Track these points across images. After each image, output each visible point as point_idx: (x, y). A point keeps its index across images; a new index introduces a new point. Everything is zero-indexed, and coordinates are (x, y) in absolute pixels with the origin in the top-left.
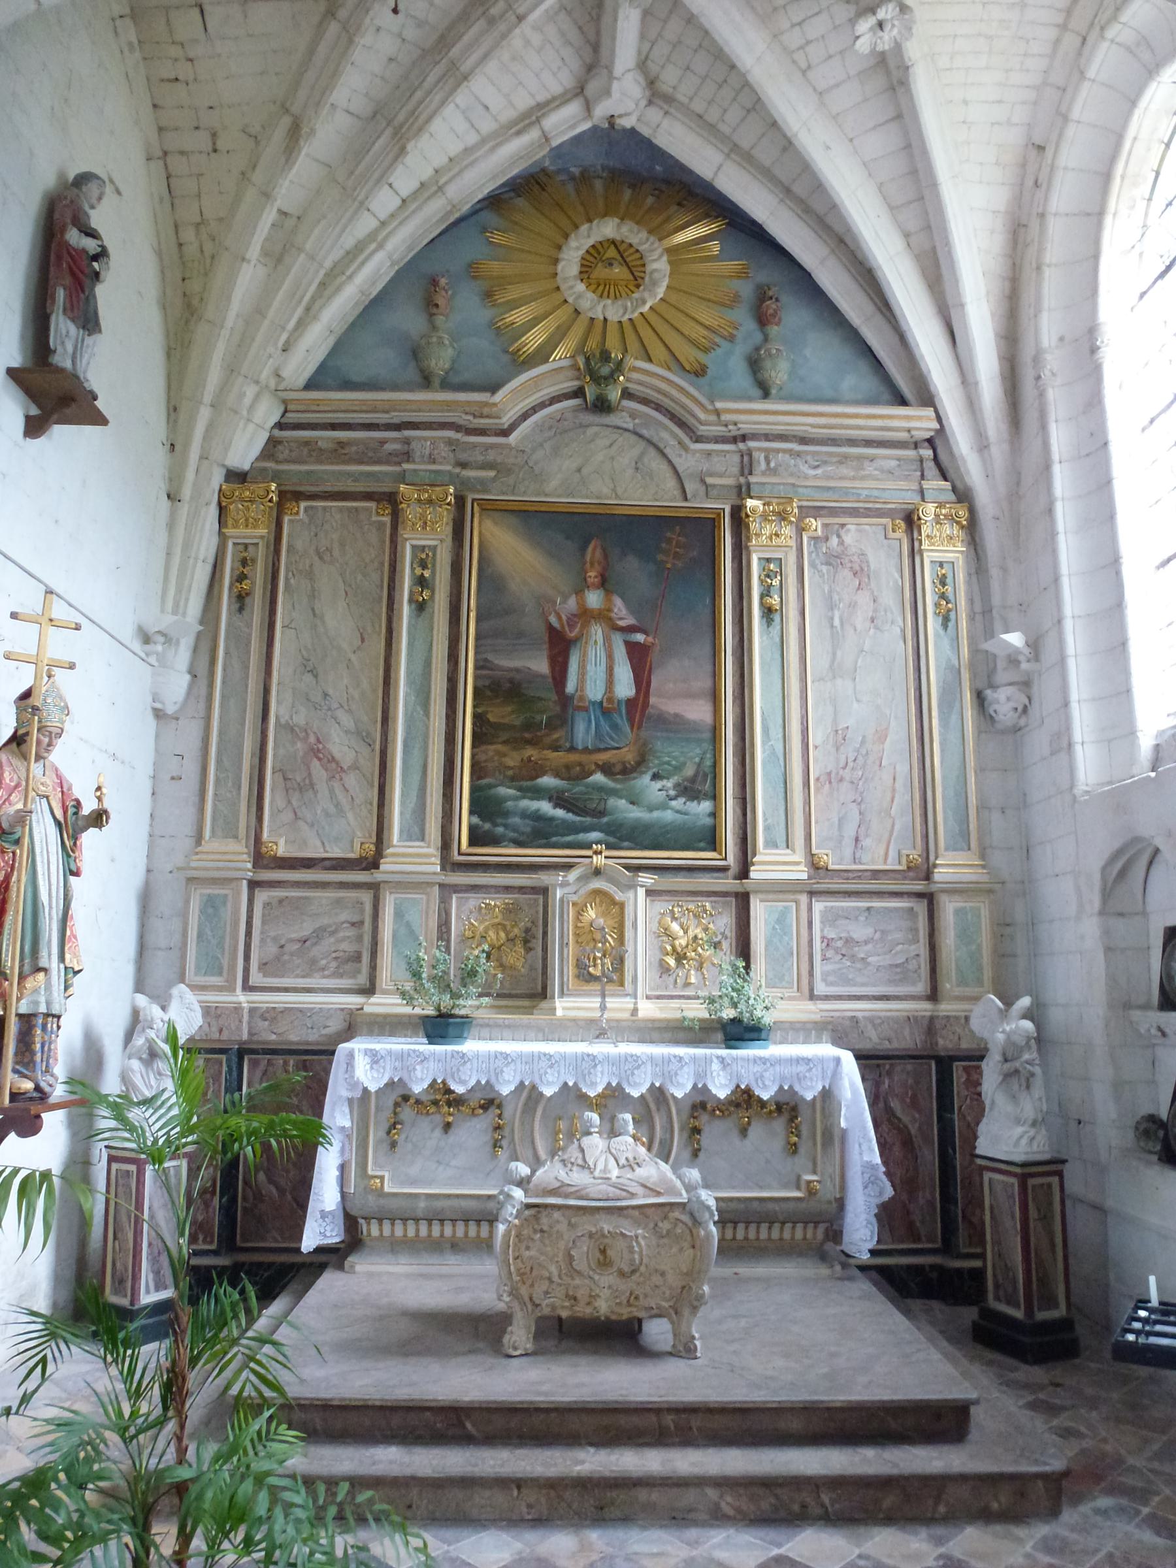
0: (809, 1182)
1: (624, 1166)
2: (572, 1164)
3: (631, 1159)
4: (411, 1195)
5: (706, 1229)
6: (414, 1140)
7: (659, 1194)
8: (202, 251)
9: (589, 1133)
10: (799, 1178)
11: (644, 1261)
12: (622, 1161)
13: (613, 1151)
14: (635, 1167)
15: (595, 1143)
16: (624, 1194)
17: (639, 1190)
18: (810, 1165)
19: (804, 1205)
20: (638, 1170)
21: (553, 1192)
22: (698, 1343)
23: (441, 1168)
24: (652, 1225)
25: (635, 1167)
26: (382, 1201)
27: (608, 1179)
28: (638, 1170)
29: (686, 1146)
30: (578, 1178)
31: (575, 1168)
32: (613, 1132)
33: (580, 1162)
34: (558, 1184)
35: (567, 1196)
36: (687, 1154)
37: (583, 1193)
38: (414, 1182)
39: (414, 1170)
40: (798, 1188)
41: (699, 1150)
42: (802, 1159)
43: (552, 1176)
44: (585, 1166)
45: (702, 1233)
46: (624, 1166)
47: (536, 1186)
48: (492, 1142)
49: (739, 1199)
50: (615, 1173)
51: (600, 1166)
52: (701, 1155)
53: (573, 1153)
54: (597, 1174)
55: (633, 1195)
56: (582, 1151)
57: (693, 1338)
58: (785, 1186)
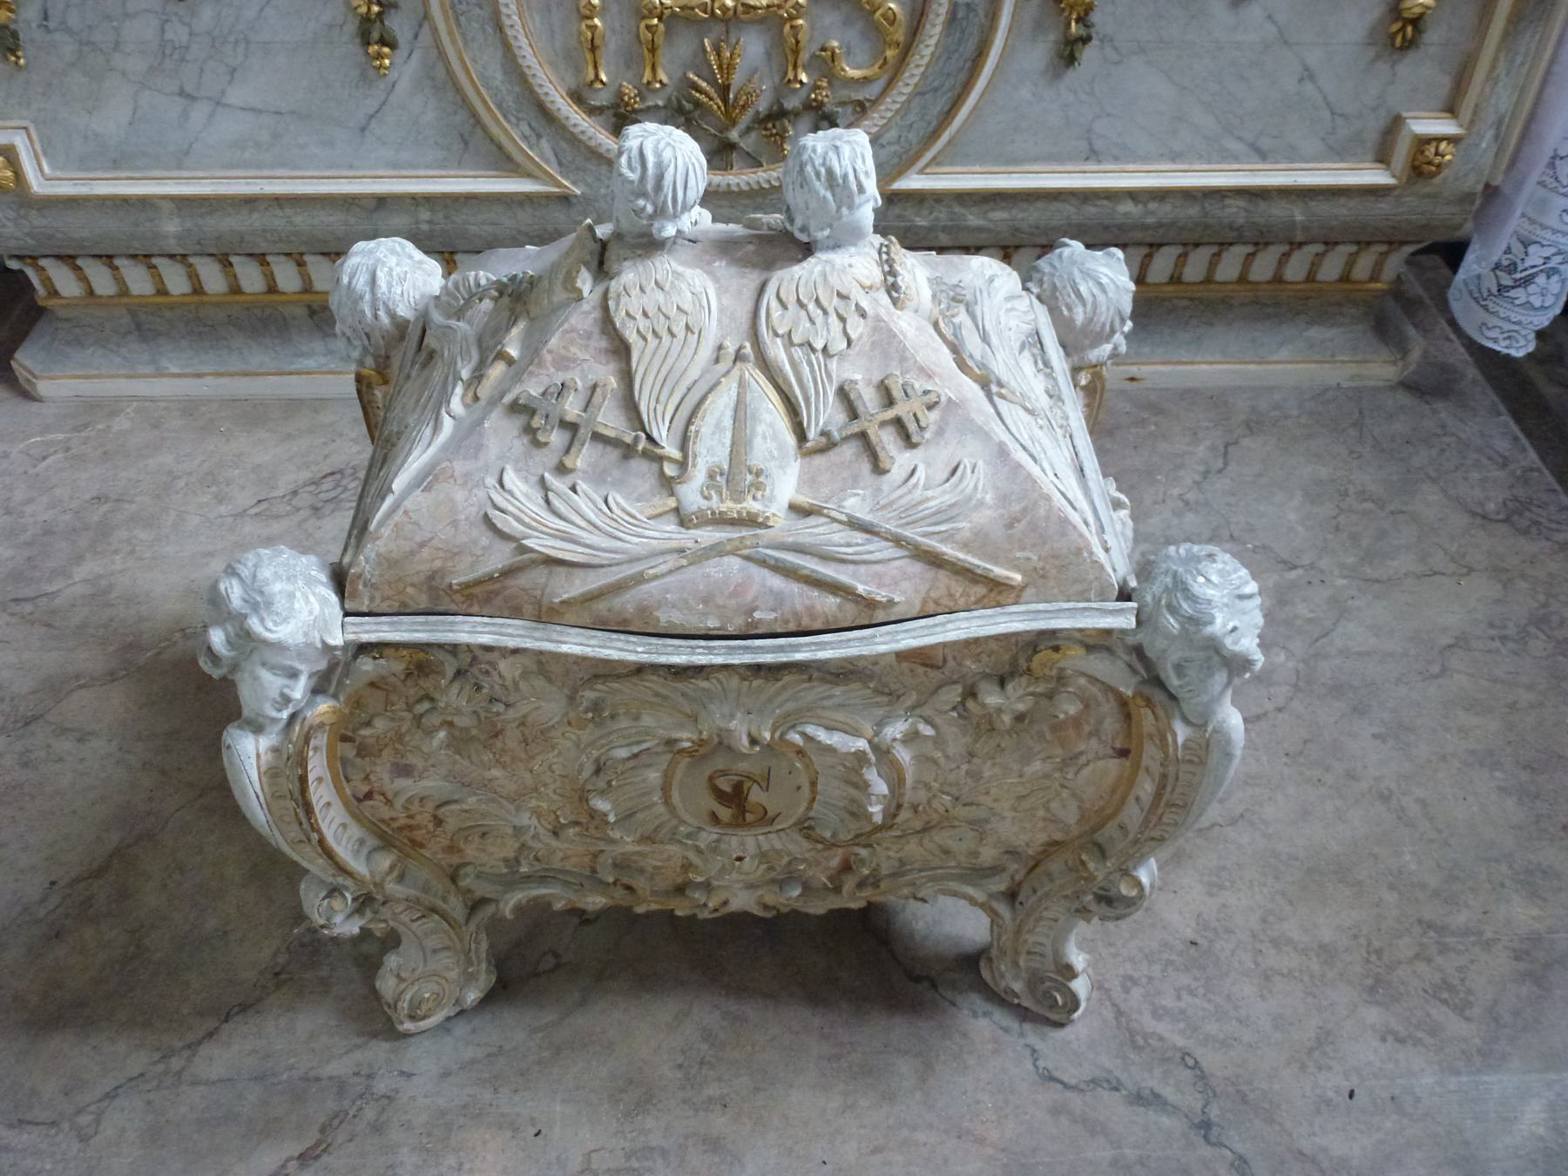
0: (1424, 141)
1: (829, 444)
2: (572, 427)
3: (868, 398)
4: (125, 201)
5: (1199, 723)
6: (74, 20)
7: (996, 592)
8: (1368, 654)
9: (649, 245)
10: (1396, 122)
11: (909, 796)
12: (825, 415)
13: (777, 351)
14: (887, 440)
15: (684, 296)
16: (829, 603)
17: (897, 582)
18: (1445, 83)
19: (1384, 206)
20: (900, 460)
21: (483, 596)
22: (1080, 986)
23: (199, 112)
24: (953, 694)
25: (887, 440)
26: (37, 220)
27: (751, 521)
28: (900, 460)
29: (1039, 27)
30: (597, 520)
31: (585, 457)
32: (774, 241)
33: (610, 420)
34: (498, 558)
35: (546, 614)
36: (1038, 53)
37: (627, 603)
38: (119, 162)
39: (112, 120)
40: (1382, 158)
41: (1086, 40)
42: (1424, 69)
43: (467, 502)
44: (634, 448)
45: (1181, 732)
46: (829, 444)
47: (389, 563)
48: (352, 27)
49: (1187, 194)
50: (786, 482)
51: (711, 449)
52: (1088, 54)
53: (572, 363)
54: (692, 494)
55: (870, 614)
56: (621, 350)
57: (1069, 972)
58: (1339, 153)
